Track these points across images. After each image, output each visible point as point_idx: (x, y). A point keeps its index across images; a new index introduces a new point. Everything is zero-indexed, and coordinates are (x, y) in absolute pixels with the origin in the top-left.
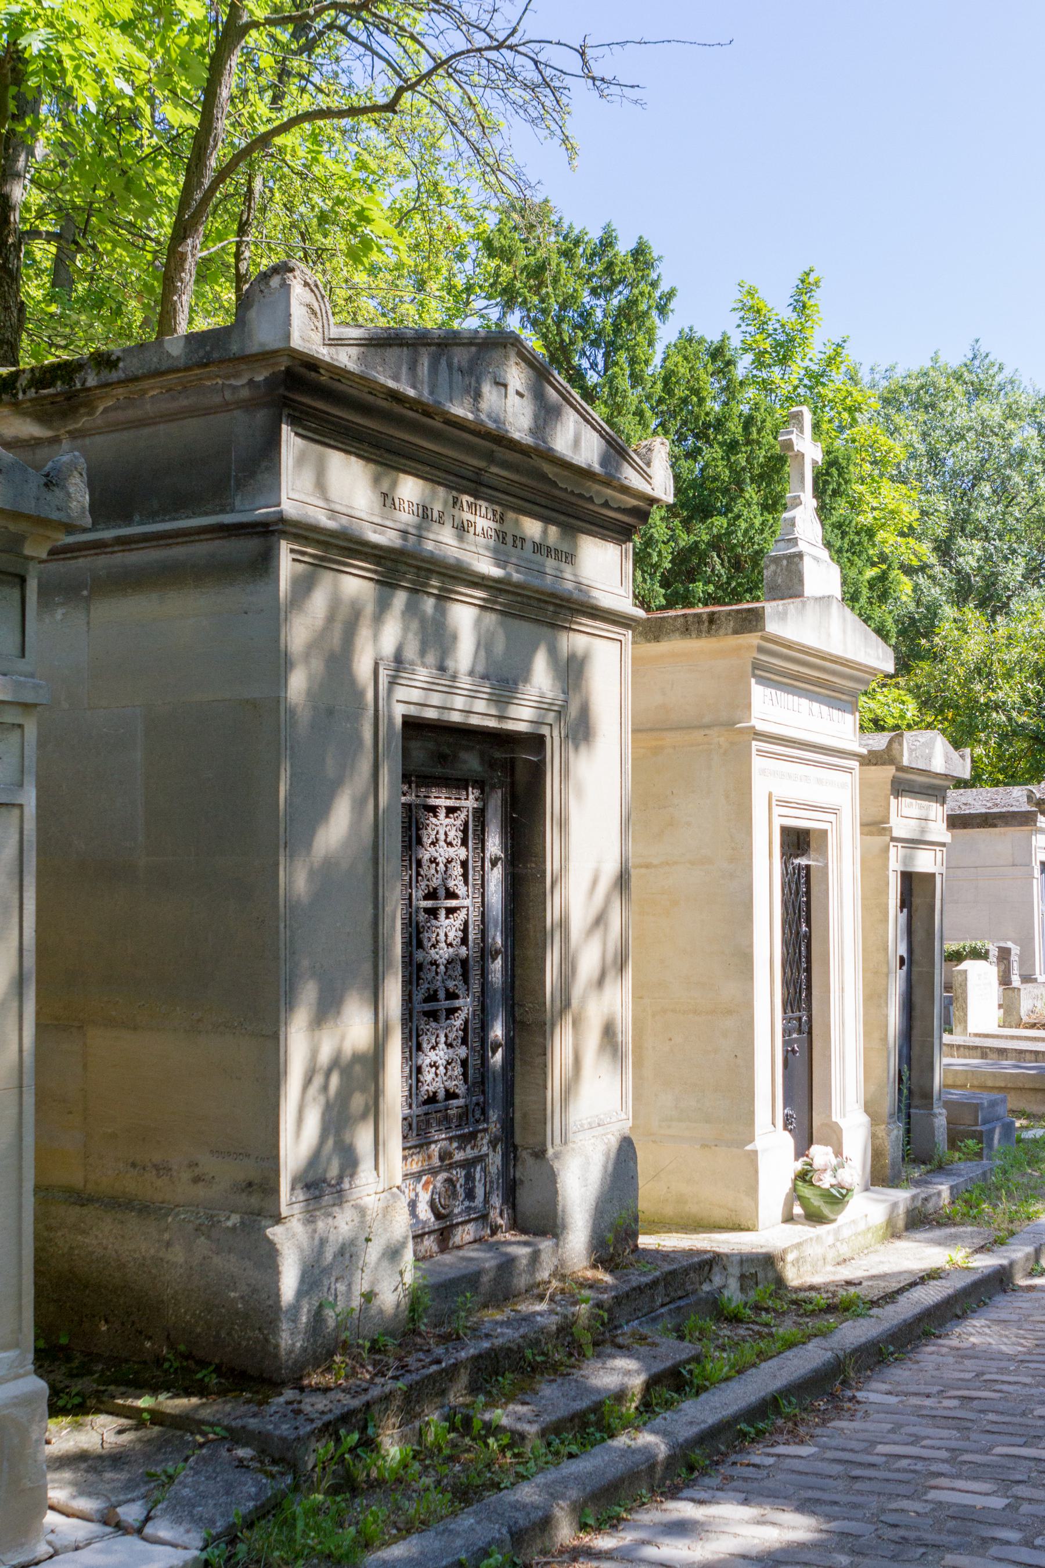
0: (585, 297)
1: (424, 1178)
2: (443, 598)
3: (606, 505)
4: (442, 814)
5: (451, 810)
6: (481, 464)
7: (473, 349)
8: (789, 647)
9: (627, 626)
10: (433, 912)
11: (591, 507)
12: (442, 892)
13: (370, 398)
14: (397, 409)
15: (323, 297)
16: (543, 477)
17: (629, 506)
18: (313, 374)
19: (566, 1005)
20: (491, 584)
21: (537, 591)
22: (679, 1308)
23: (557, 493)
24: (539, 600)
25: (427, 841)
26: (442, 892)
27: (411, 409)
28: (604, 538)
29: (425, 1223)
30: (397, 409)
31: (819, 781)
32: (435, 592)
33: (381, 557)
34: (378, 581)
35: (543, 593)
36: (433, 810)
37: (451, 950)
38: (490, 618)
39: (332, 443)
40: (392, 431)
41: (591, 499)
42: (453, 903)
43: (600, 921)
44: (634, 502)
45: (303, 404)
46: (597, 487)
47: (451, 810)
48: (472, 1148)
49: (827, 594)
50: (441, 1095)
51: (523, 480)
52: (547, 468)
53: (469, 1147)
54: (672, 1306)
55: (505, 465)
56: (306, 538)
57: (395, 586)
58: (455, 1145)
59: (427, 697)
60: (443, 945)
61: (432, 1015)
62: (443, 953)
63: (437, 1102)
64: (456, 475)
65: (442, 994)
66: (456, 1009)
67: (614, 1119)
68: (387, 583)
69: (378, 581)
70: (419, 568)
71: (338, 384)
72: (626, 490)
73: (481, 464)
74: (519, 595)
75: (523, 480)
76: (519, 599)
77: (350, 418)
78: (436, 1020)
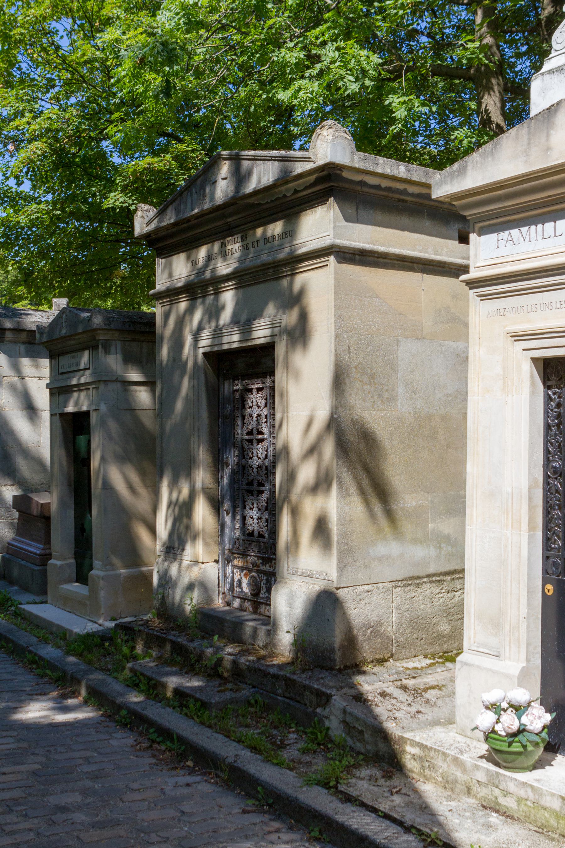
1: (245, 572)
2: (217, 293)
3: (296, 191)
4: (254, 392)
5: (259, 390)
8: (538, 178)
9: (328, 254)
10: (250, 441)
11: (288, 199)
12: (255, 431)
13: (170, 231)
16: (253, 205)
17: (312, 182)
19: (287, 498)
20: (232, 276)
22: (289, 704)
23: (265, 207)
25: (247, 406)
26: (255, 431)
28: (312, 207)
29: (246, 594)
31: (550, 306)
32: (212, 292)
36: (251, 391)
37: (260, 461)
40: (191, 234)
41: (285, 196)
42: (260, 437)
43: (313, 450)
44: (314, 177)
46: (283, 188)
47: (259, 390)
48: (270, 567)
49: (555, 101)
50: (256, 533)
51: (244, 214)
52: (251, 201)
53: (268, 565)
54: (286, 700)
55: (231, 215)
57: (196, 299)
58: (260, 561)
60: (255, 458)
61: (251, 492)
62: (255, 462)
63: (253, 536)
64: (220, 233)
65: (255, 483)
66: (262, 492)
67: (322, 577)
68: (193, 299)
72: (300, 176)
75: (244, 214)
76: (251, 275)
78: (252, 495)
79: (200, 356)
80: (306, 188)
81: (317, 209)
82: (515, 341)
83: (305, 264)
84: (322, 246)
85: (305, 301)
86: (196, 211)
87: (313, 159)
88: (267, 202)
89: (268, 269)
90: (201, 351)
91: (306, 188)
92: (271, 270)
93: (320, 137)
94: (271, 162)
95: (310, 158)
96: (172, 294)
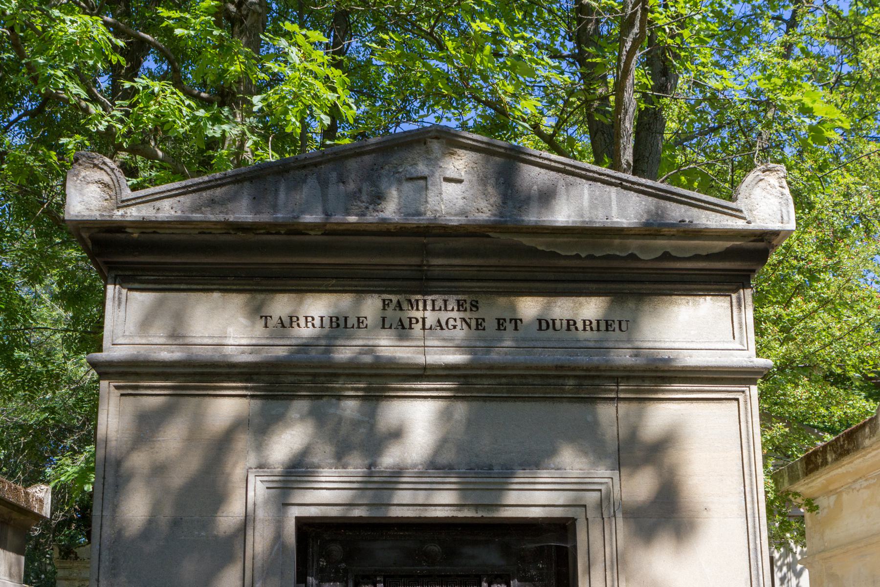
0: (362, 53)
6: (415, 260)
7: (367, 159)
14: (251, 237)
15: (112, 170)
16: (532, 252)
17: (717, 250)
18: (123, 236)
21: (307, 367)
23: (563, 263)
24: (541, 376)
27: (269, 233)
30: (251, 237)
33: (251, 374)
34: (252, 396)
35: (543, 368)
38: (461, 409)
39: (201, 287)
45: (121, 263)
56: (137, 374)
59: (427, 497)
64: (494, 280)
69: (252, 396)
70: (315, 375)
71: (156, 236)
73: (415, 260)
74: (505, 376)
76: (504, 380)
77: (196, 261)
79: (290, 528)
80: (697, 257)
81: (701, 300)
82: (122, 395)
83: (676, 387)
84: (744, 364)
85: (672, 456)
86: (353, 219)
87: (745, 214)
88: (578, 256)
89: (568, 377)
90: (295, 512)
91: (697, 257)
92: (571, 382)
93: (761, 184)
94: (613, 189)
95: (741, 211)
96: (189, 374)
